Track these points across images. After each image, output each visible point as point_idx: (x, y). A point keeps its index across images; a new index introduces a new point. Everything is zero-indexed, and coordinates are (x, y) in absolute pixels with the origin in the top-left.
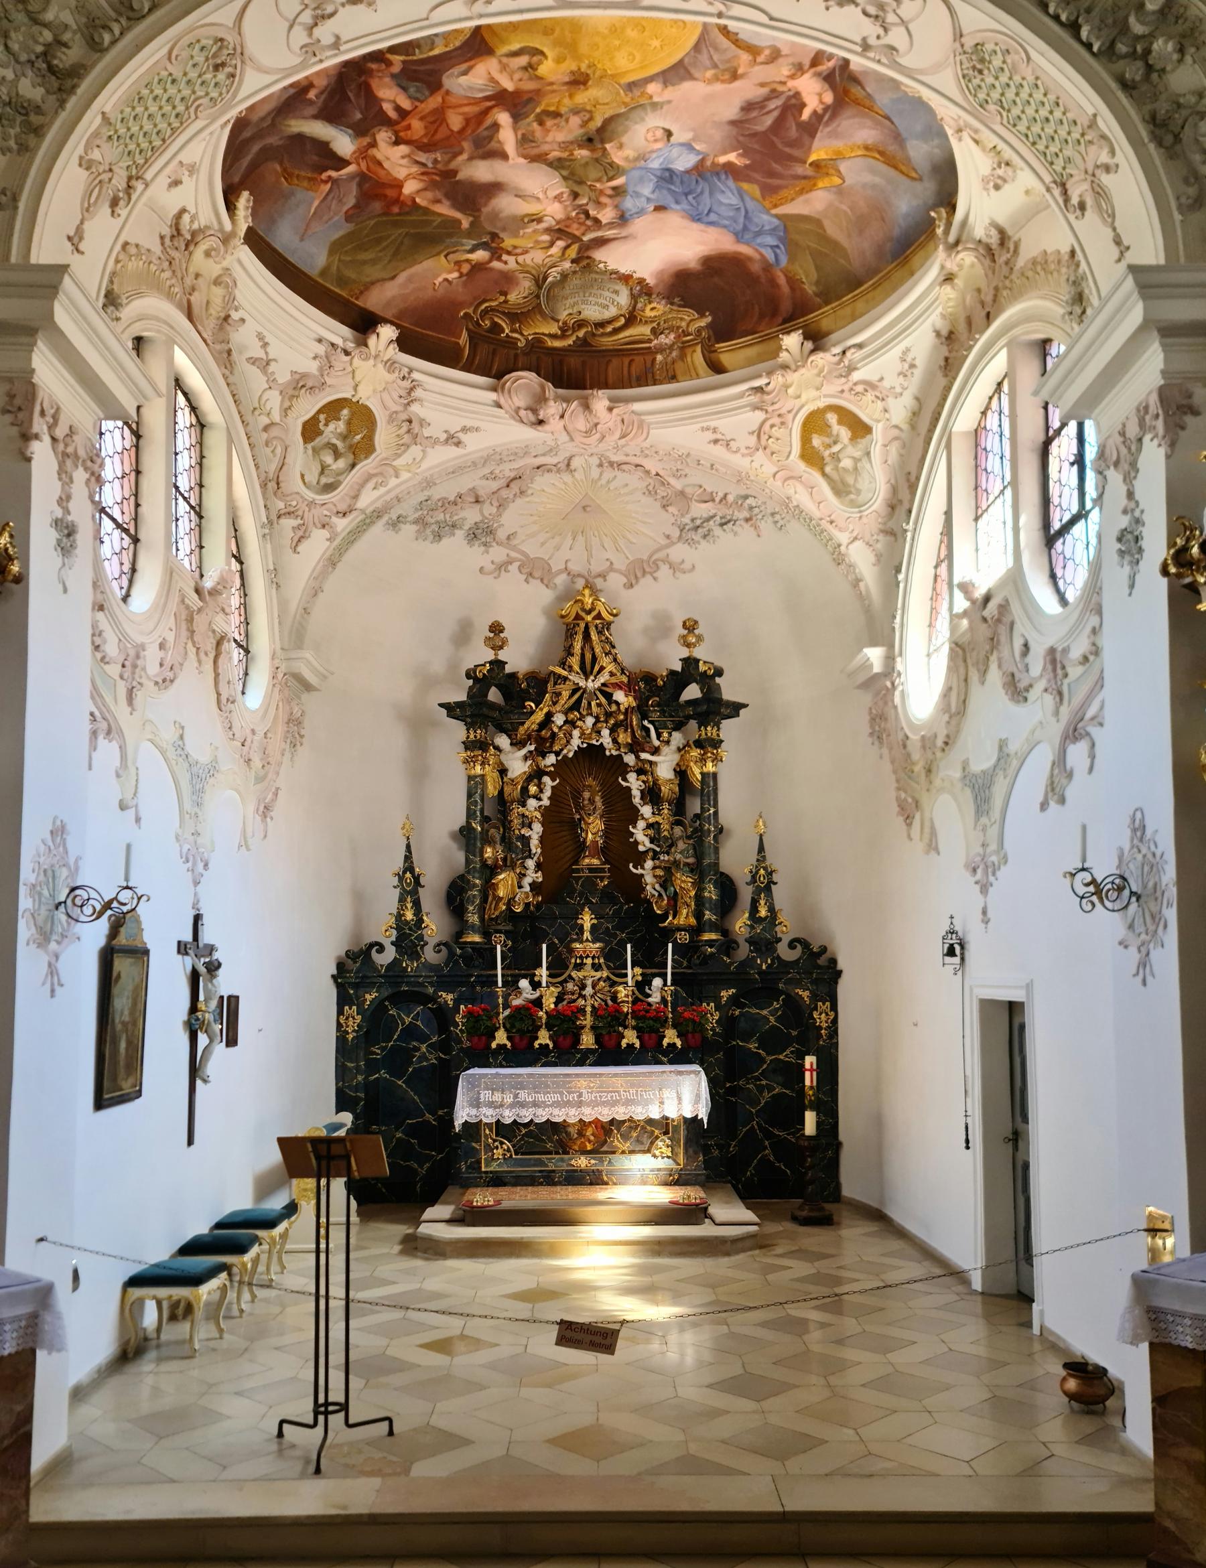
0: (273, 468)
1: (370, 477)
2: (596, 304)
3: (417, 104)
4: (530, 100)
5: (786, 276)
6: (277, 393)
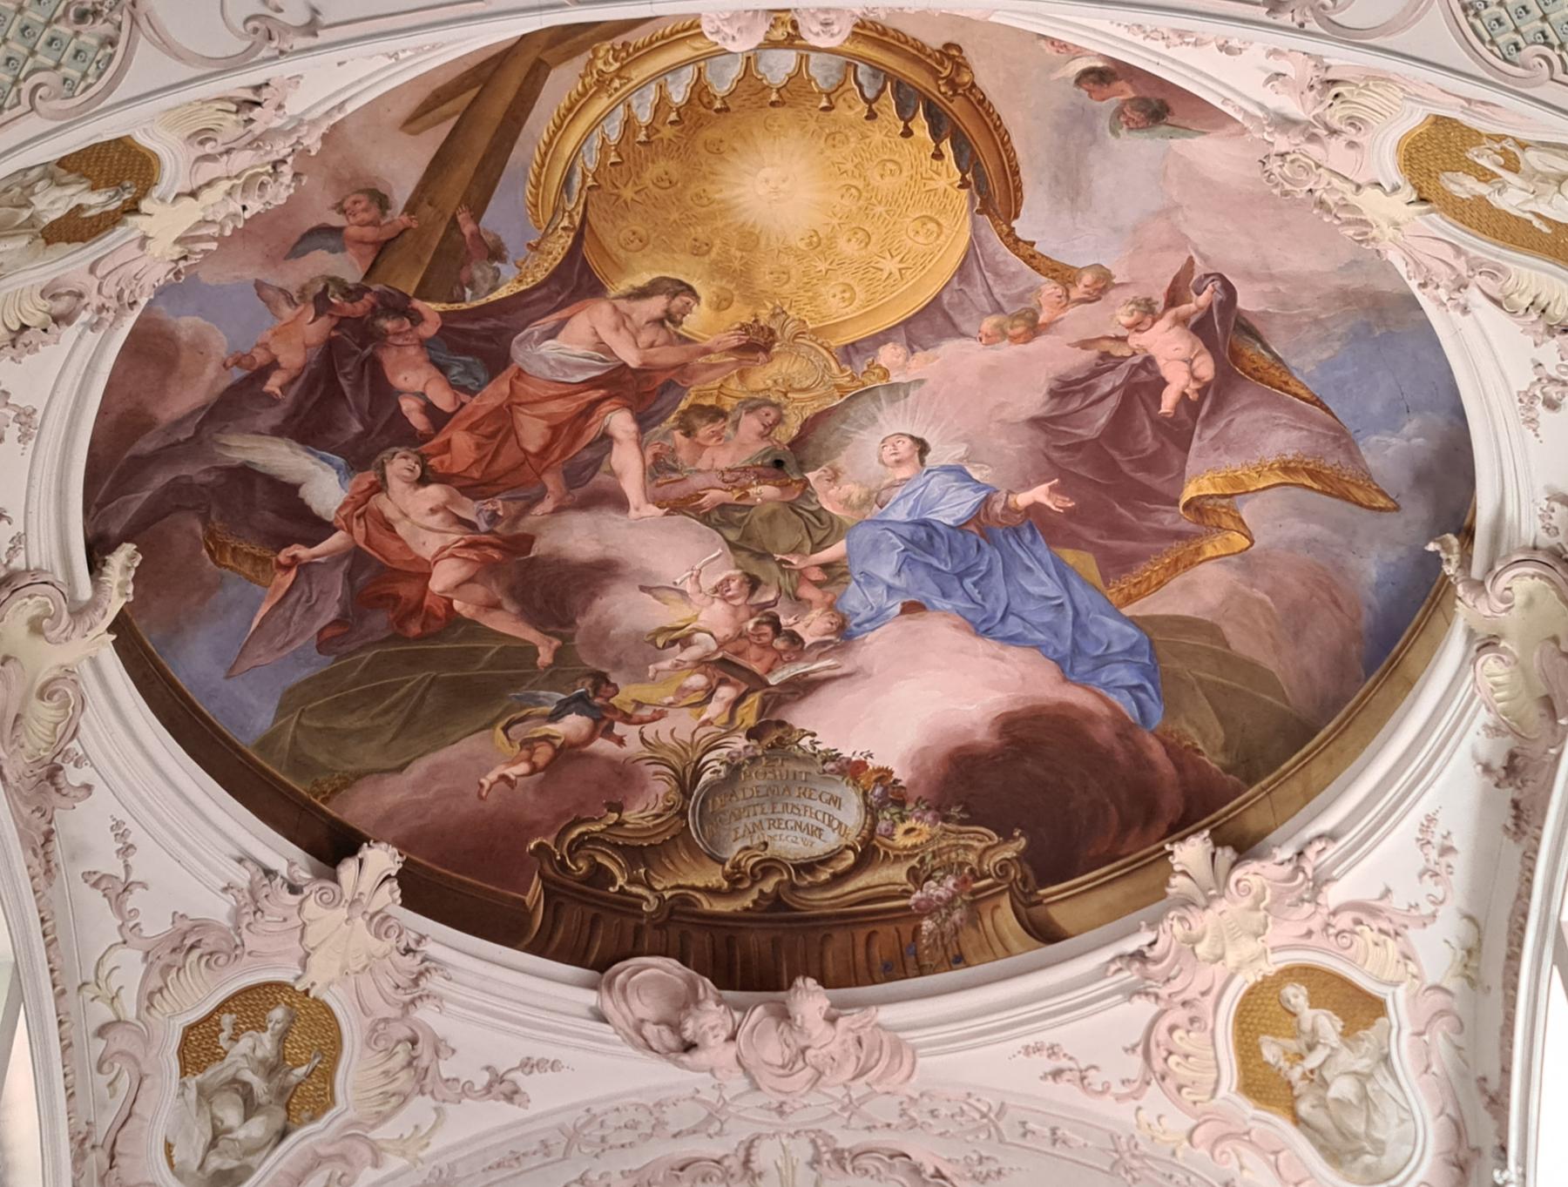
0: (105, 1123)
1: (318, 1161)
2: (798, 825)
3: (465, 398)
4: (669, 385)
5: (1164, 743)
6: (140, 954)
